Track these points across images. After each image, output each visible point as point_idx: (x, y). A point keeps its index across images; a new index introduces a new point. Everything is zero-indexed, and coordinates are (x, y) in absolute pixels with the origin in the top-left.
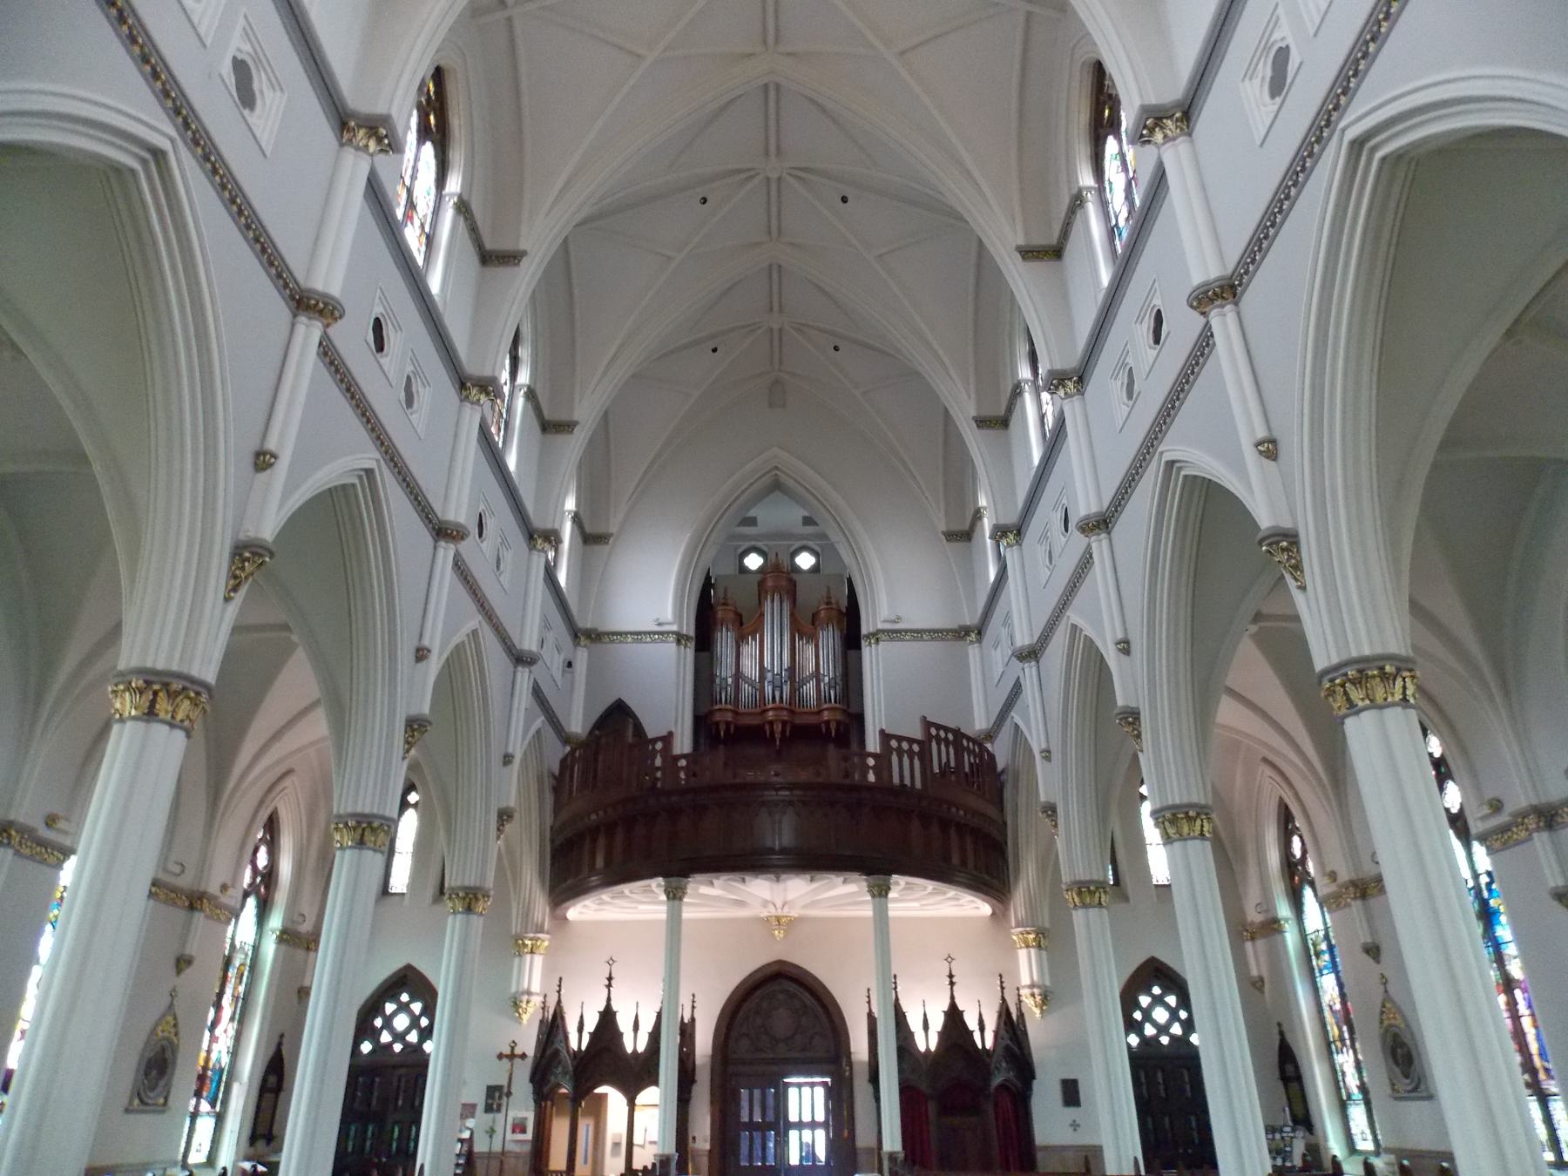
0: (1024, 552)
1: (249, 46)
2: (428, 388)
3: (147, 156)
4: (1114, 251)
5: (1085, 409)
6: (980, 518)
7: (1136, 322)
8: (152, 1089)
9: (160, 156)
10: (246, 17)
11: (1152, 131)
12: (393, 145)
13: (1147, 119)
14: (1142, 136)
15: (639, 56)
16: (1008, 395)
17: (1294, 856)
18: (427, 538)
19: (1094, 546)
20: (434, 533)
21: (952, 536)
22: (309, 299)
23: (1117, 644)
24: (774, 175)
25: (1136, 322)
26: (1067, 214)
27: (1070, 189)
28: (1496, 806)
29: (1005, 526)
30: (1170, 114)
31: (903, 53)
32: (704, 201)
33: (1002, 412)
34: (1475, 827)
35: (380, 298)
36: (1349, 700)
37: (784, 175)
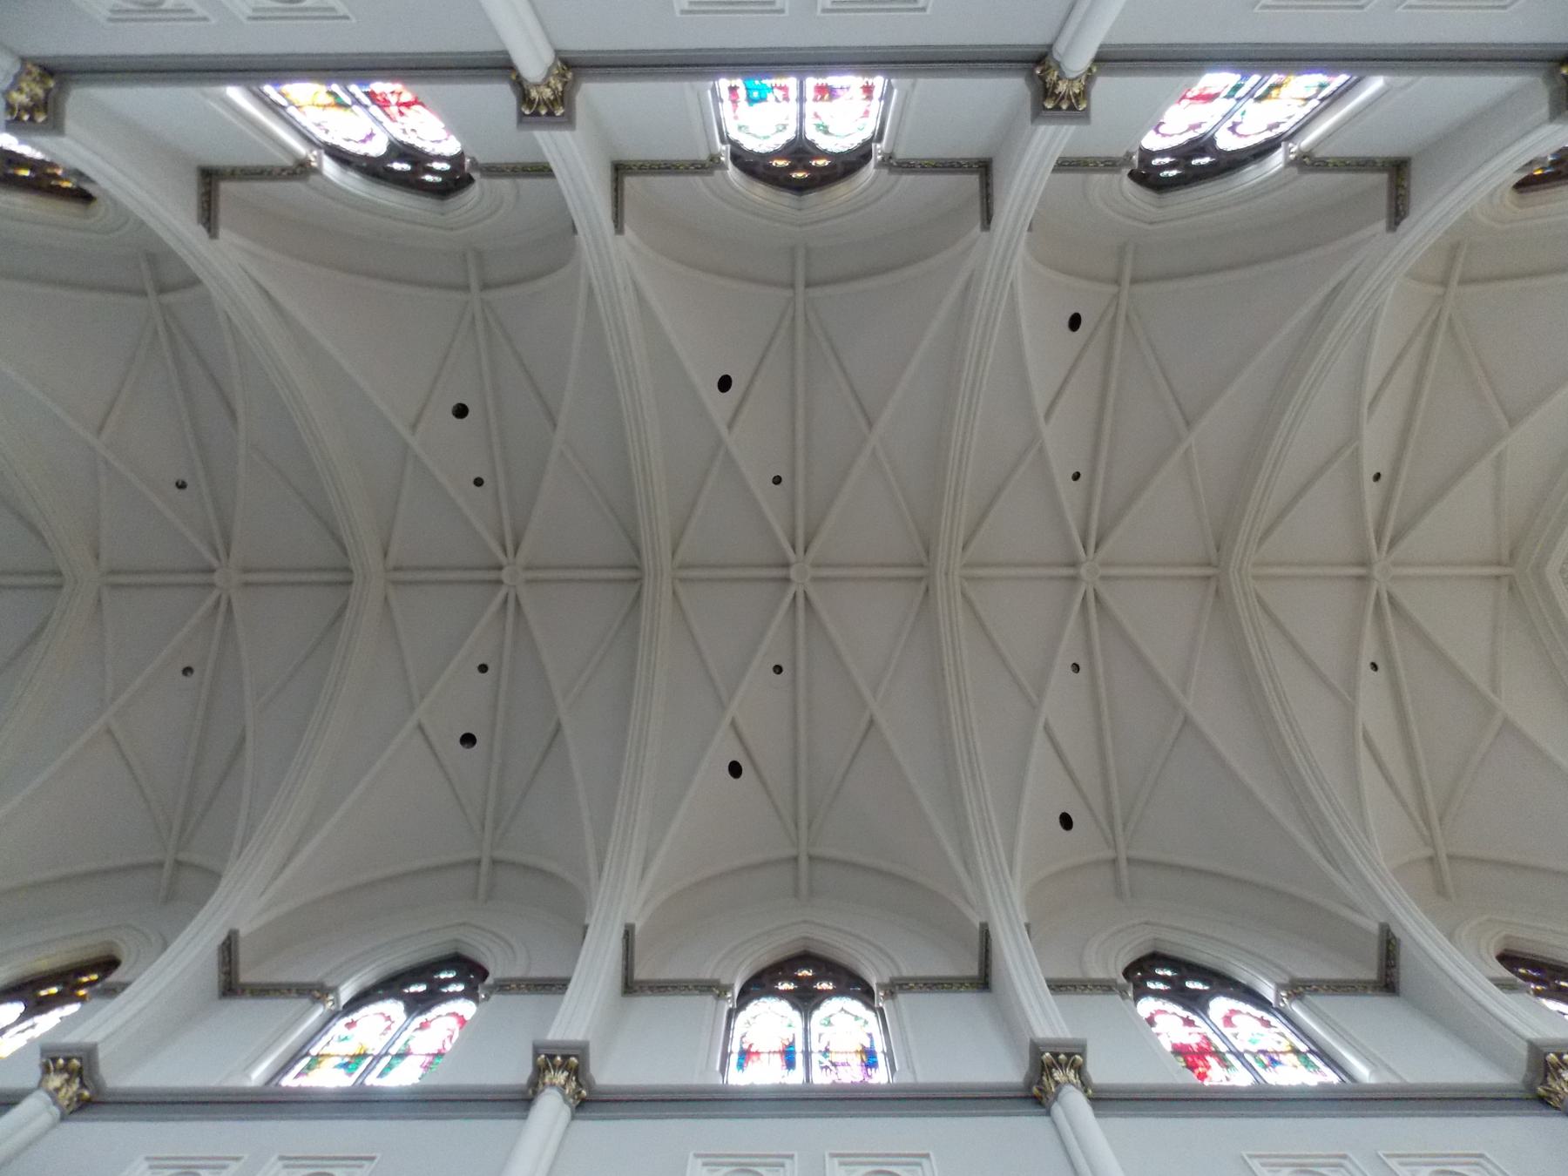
2: (109, 14)
10: (205, 19)
11: (64, 1069)
13: (576, 1056)
14: (55, 1060)
15: (101, 429)
24: (505, 575)
25: (147, 1159)
30: (583, 1083)
31: (109, 732)
32: (181, 486)
37: (216, 593)
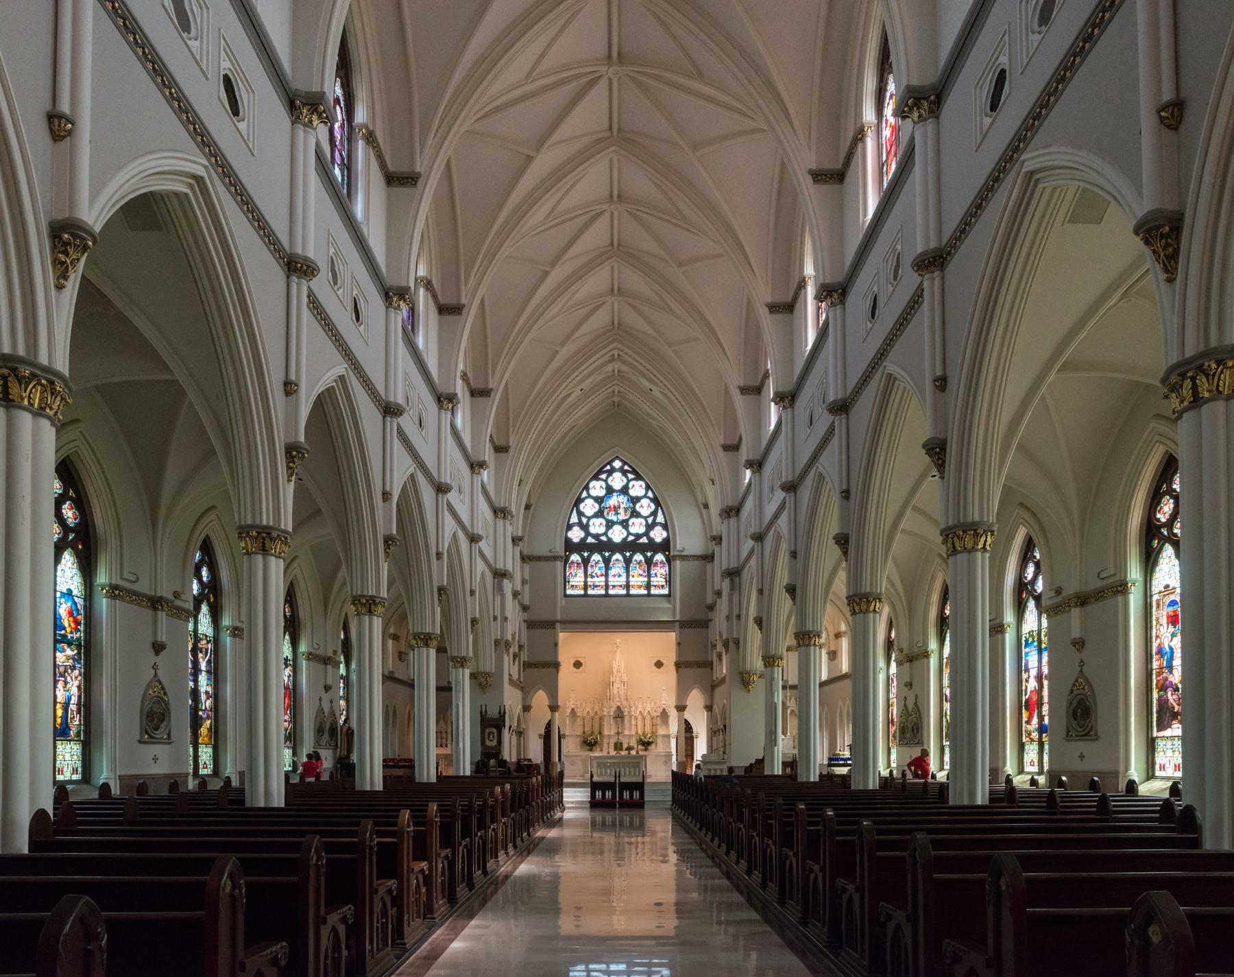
0: (796, 413)
1: (229, 63)
3: (192, 181)
4: (881, 181)
5: (844, 316)
6: (768, 377)
7: (976, 87)
8: (157, 728)
9: (200, 181)
11: (911, 110)
12: (330, 118)
13: (909, 99)
16: (795, 286)
17: (1026, 578)
18: (278, 273)
19: (926, 285)
20: (286, 268)
21: (726, 448)
22: (296, 263)
23: (842, 492)
26: (851, 145)
27: (855, 124)
28: (1059, 591)
29: (752, 461)
33: (789, 299)
34: (1044, 603)
35: (225, 50)
36: (954, 547)
